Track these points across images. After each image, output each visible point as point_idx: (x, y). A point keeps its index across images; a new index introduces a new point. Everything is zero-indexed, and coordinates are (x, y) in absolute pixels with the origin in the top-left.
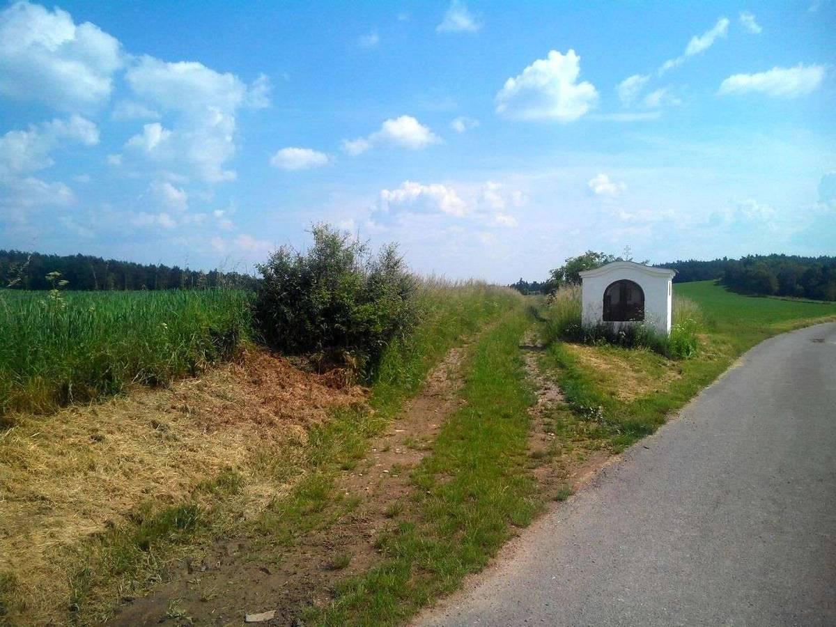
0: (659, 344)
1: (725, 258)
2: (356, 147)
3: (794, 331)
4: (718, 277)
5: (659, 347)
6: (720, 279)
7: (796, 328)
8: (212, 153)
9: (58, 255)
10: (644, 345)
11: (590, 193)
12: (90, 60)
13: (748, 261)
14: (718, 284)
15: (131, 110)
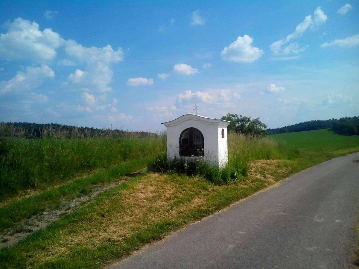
0: (211, 173)
1: (333, 119)
2: (163, 76)
3: (348, 155)
4: (330, 127)
5: (211, 175)
6: (331, 128)
7: (351, 153)
8: (103, 79)
9: (43, 124)
10: (201, 174)
11: (267, 92)
12: (48, 43)
13: (342, 120)
14: (330, 130)
15: (67, 63)
